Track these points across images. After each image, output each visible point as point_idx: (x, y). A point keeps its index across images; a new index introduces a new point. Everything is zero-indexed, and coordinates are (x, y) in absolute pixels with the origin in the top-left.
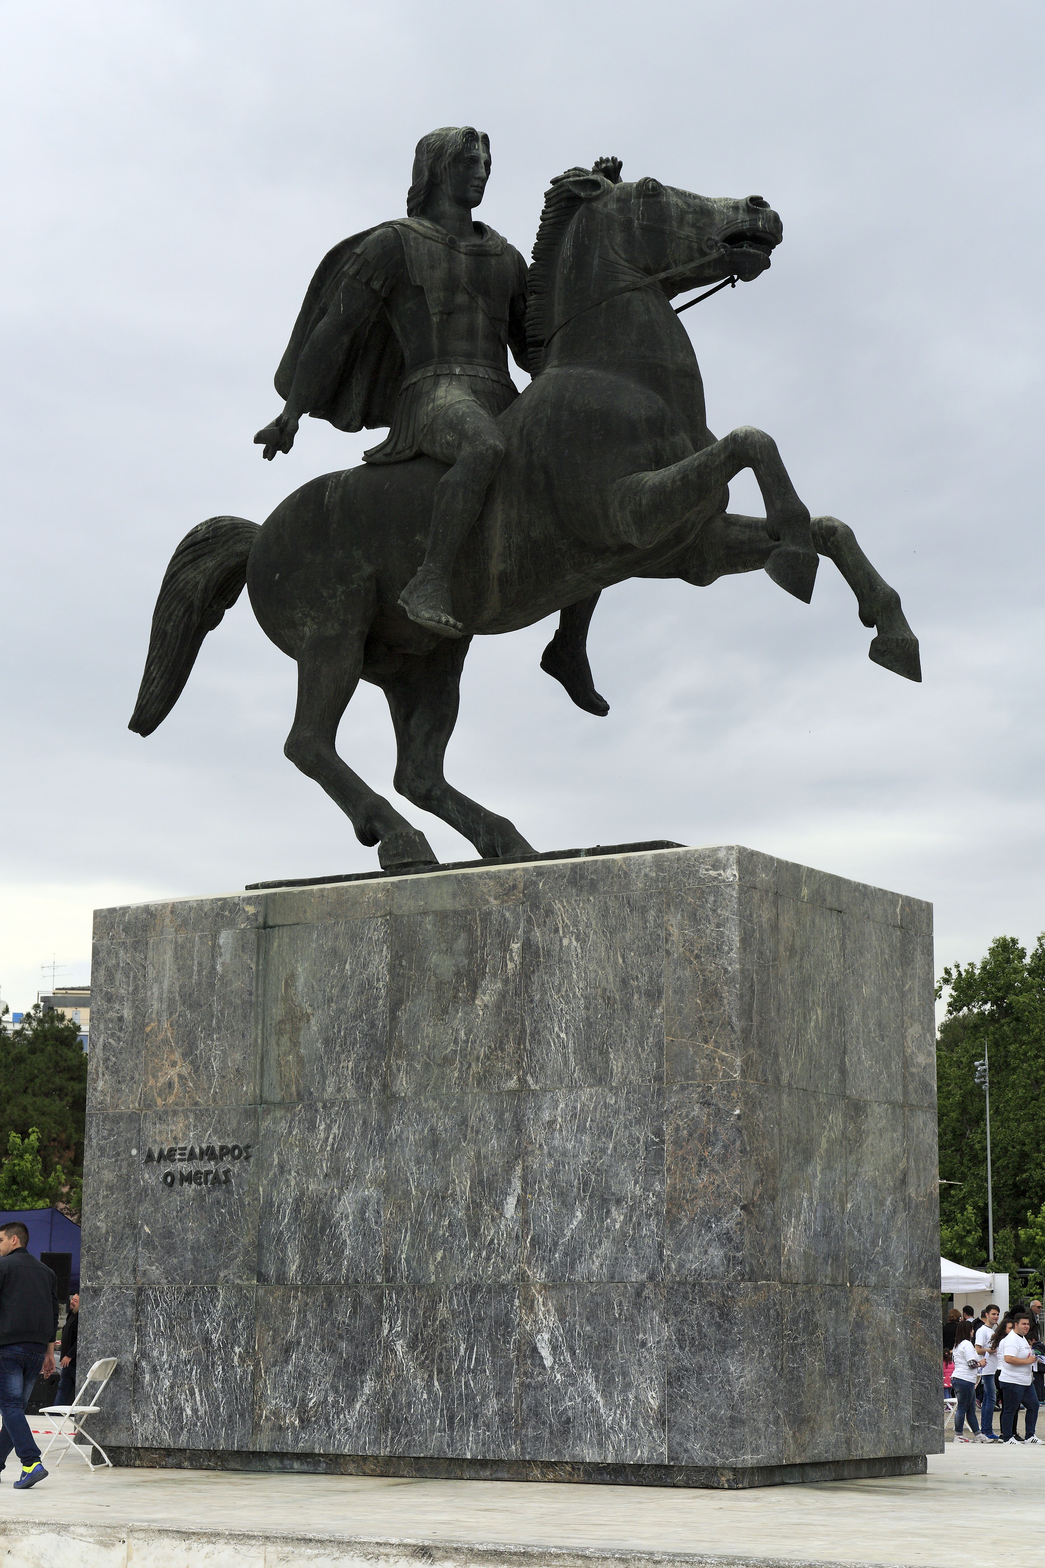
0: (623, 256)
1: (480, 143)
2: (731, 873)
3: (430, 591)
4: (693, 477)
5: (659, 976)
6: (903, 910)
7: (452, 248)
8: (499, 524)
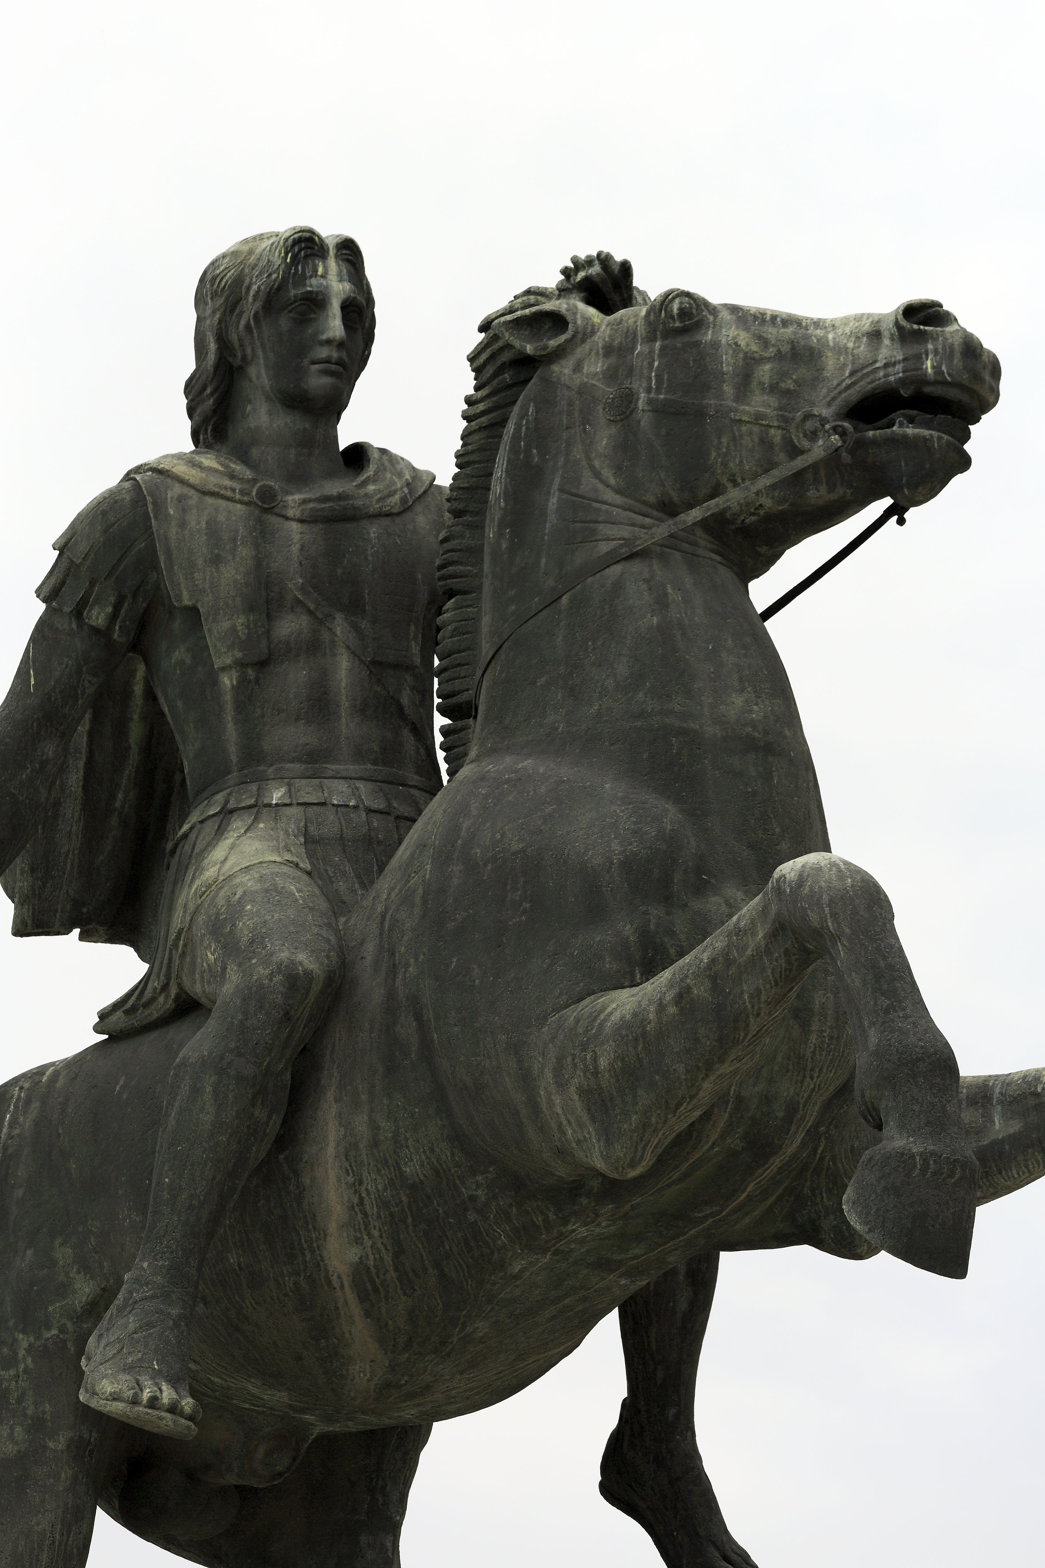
0: (612, 481)
1: (332, 262)
3: (131, 1327)
4: (701, 991)
7: (267, 511)
8: (331, 1150)
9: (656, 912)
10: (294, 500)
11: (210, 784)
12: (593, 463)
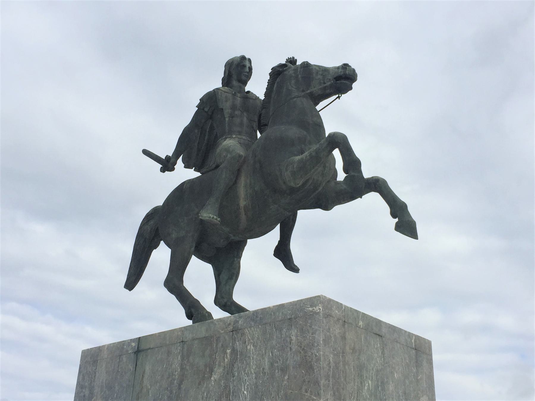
4: (314, 154)
5: (287, 360)
6: (415, 341)
9: (303, 146)
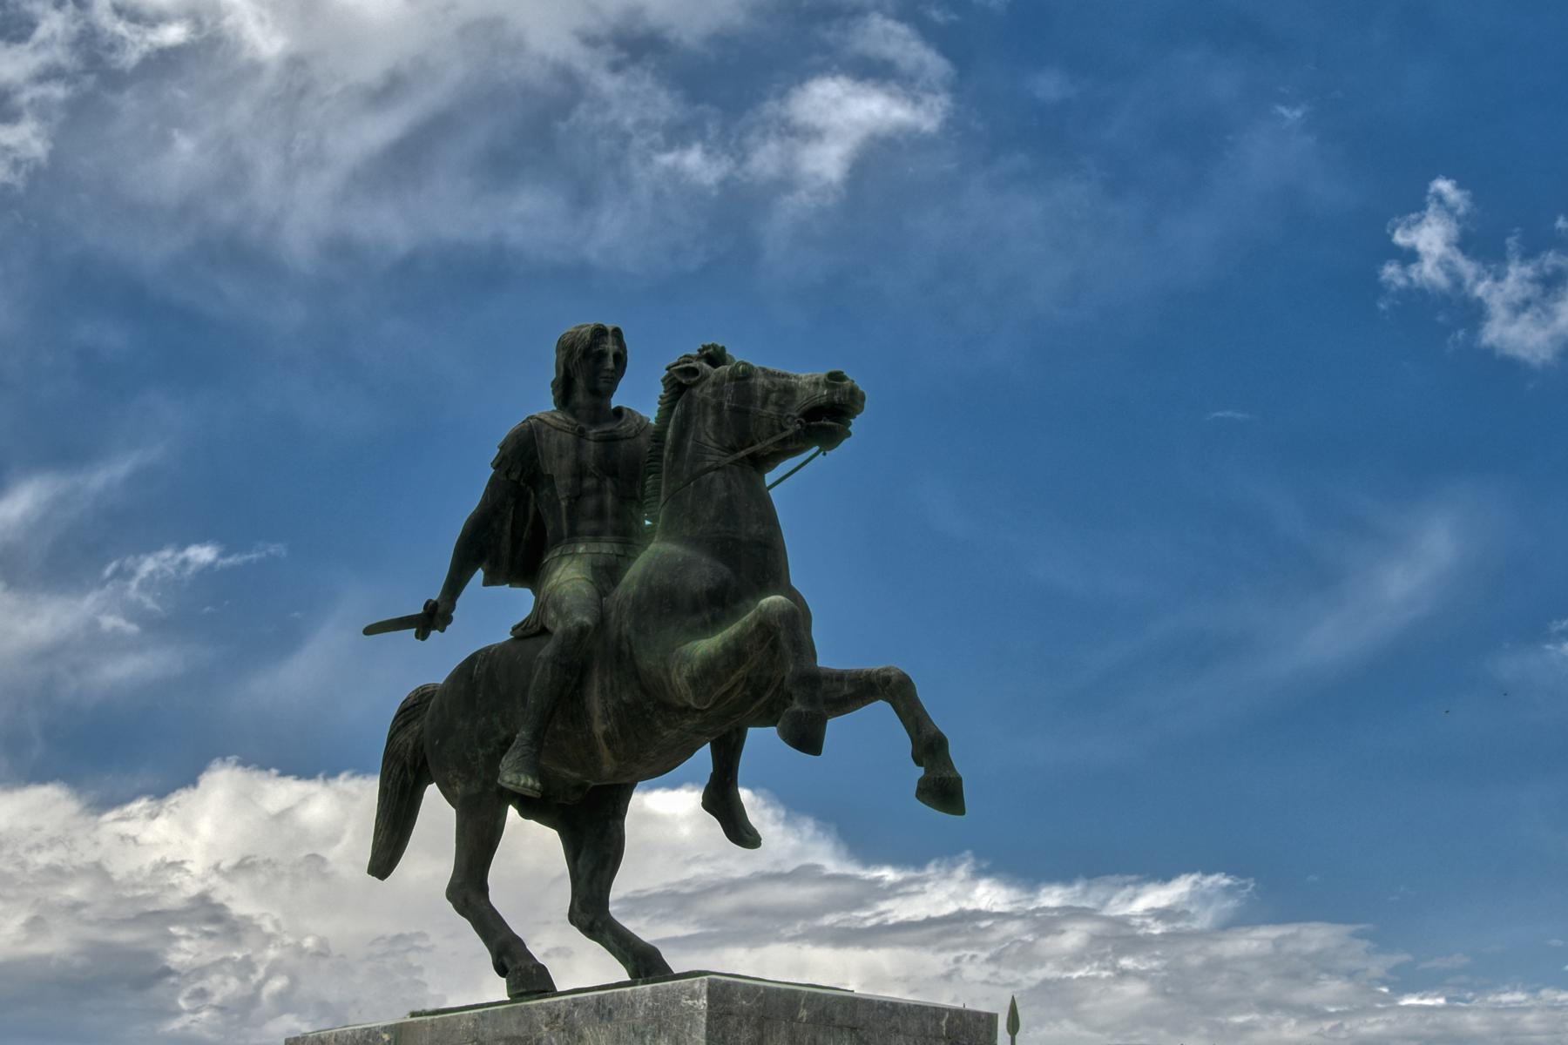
1: (610, 338)
2: (702, 1003)
10: (593, 432)
11: (558, 541)
12: (706, 430)
